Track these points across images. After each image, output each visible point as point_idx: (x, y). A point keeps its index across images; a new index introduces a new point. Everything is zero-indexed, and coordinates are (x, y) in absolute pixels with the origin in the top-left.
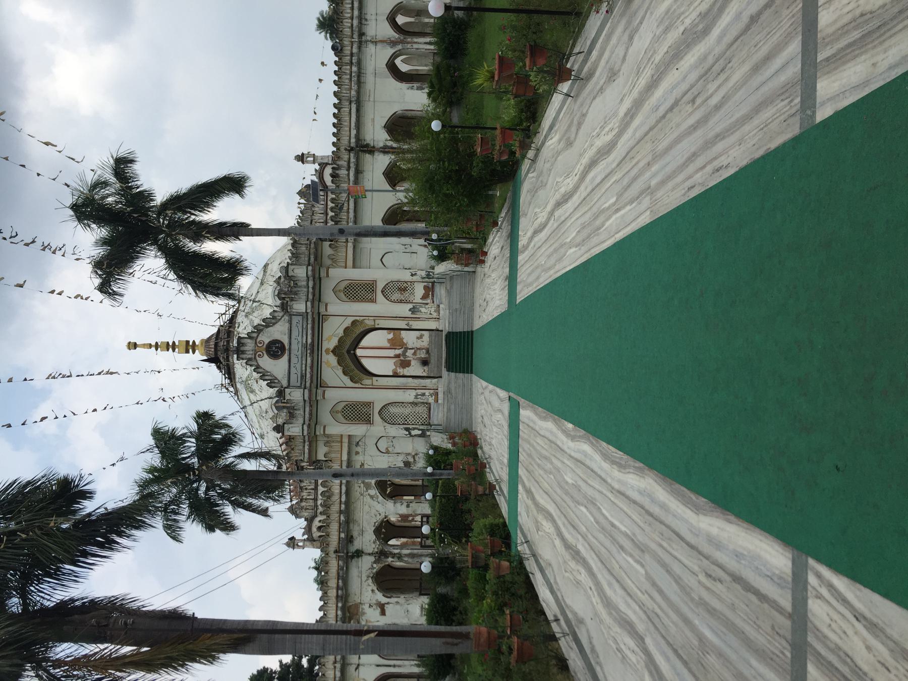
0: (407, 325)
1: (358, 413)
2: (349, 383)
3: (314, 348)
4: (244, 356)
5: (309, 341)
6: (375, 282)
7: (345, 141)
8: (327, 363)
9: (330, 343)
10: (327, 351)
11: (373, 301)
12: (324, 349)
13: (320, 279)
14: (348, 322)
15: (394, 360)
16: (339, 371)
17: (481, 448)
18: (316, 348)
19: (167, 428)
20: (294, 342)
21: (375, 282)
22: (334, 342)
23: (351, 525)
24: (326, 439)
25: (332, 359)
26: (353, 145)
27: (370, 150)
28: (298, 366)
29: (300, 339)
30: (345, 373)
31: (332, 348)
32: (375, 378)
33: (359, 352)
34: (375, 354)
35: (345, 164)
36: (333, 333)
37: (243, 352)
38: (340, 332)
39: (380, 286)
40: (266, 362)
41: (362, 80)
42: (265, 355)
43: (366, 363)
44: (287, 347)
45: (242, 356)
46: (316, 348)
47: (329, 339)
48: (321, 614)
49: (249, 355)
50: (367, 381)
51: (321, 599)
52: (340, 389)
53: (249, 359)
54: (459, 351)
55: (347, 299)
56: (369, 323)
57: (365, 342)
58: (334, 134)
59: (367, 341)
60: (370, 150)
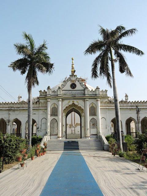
0: (83, 127)
1: (54, 112)
2: (63, 109)
3: (74, 97)
4: (71, 77)
5: (76, 96)
6: (57, 115)
7: (139, 105)
8: (69, 102)
9: (76, 102)
10: (73, 102)
11: (51, 115)
12: (74, 100)
13: (96, 99)
14: (83, 108)
15: (71, 124)
16: (67, 106)
17: (110, 159)
18: (74, 98)
19: (99, 51)
20: (76, 91)
21: (57, 115)
22: (76, 103)
23: (19, 111)
24: (46, 102)
25: (71, 103)
26: (139, 107)
27: (138, 112)
28: (68, 93)
29: (77, 93)
30: (67, 107)
31: (74, 103)
32: (65, 117)
33: (73, 113)
34: (74, 117)
35: (132, 105)
36: (80, 103)
37: (72, 77)
38: (79, 105)
39: (56, 118)
40: (69, 83)
41: (131, 110)
42: (71, 83)
43: (70, 115)
44: (74, 89)
45: (71, 76)
46: (74, 98)
47: (77, 102)
48: (2, 103)
49: (71, 78)
50: (64, 114)
51: (5, 102)
52: (62, 106)
53: (70, 79)
54: (71, 146)
55: (51, 108)
56: (83, 114)
57: (76, 114)
58: (141, 101)
59: (77, 115)
60: (138, 112)
